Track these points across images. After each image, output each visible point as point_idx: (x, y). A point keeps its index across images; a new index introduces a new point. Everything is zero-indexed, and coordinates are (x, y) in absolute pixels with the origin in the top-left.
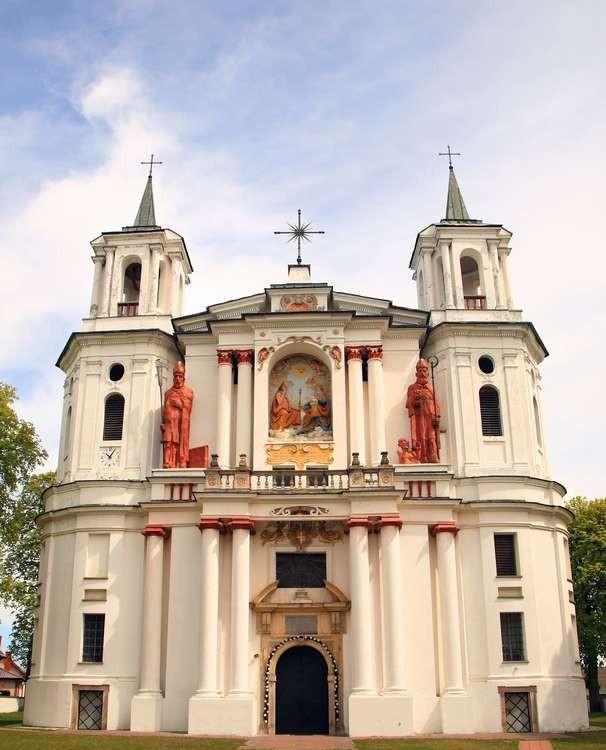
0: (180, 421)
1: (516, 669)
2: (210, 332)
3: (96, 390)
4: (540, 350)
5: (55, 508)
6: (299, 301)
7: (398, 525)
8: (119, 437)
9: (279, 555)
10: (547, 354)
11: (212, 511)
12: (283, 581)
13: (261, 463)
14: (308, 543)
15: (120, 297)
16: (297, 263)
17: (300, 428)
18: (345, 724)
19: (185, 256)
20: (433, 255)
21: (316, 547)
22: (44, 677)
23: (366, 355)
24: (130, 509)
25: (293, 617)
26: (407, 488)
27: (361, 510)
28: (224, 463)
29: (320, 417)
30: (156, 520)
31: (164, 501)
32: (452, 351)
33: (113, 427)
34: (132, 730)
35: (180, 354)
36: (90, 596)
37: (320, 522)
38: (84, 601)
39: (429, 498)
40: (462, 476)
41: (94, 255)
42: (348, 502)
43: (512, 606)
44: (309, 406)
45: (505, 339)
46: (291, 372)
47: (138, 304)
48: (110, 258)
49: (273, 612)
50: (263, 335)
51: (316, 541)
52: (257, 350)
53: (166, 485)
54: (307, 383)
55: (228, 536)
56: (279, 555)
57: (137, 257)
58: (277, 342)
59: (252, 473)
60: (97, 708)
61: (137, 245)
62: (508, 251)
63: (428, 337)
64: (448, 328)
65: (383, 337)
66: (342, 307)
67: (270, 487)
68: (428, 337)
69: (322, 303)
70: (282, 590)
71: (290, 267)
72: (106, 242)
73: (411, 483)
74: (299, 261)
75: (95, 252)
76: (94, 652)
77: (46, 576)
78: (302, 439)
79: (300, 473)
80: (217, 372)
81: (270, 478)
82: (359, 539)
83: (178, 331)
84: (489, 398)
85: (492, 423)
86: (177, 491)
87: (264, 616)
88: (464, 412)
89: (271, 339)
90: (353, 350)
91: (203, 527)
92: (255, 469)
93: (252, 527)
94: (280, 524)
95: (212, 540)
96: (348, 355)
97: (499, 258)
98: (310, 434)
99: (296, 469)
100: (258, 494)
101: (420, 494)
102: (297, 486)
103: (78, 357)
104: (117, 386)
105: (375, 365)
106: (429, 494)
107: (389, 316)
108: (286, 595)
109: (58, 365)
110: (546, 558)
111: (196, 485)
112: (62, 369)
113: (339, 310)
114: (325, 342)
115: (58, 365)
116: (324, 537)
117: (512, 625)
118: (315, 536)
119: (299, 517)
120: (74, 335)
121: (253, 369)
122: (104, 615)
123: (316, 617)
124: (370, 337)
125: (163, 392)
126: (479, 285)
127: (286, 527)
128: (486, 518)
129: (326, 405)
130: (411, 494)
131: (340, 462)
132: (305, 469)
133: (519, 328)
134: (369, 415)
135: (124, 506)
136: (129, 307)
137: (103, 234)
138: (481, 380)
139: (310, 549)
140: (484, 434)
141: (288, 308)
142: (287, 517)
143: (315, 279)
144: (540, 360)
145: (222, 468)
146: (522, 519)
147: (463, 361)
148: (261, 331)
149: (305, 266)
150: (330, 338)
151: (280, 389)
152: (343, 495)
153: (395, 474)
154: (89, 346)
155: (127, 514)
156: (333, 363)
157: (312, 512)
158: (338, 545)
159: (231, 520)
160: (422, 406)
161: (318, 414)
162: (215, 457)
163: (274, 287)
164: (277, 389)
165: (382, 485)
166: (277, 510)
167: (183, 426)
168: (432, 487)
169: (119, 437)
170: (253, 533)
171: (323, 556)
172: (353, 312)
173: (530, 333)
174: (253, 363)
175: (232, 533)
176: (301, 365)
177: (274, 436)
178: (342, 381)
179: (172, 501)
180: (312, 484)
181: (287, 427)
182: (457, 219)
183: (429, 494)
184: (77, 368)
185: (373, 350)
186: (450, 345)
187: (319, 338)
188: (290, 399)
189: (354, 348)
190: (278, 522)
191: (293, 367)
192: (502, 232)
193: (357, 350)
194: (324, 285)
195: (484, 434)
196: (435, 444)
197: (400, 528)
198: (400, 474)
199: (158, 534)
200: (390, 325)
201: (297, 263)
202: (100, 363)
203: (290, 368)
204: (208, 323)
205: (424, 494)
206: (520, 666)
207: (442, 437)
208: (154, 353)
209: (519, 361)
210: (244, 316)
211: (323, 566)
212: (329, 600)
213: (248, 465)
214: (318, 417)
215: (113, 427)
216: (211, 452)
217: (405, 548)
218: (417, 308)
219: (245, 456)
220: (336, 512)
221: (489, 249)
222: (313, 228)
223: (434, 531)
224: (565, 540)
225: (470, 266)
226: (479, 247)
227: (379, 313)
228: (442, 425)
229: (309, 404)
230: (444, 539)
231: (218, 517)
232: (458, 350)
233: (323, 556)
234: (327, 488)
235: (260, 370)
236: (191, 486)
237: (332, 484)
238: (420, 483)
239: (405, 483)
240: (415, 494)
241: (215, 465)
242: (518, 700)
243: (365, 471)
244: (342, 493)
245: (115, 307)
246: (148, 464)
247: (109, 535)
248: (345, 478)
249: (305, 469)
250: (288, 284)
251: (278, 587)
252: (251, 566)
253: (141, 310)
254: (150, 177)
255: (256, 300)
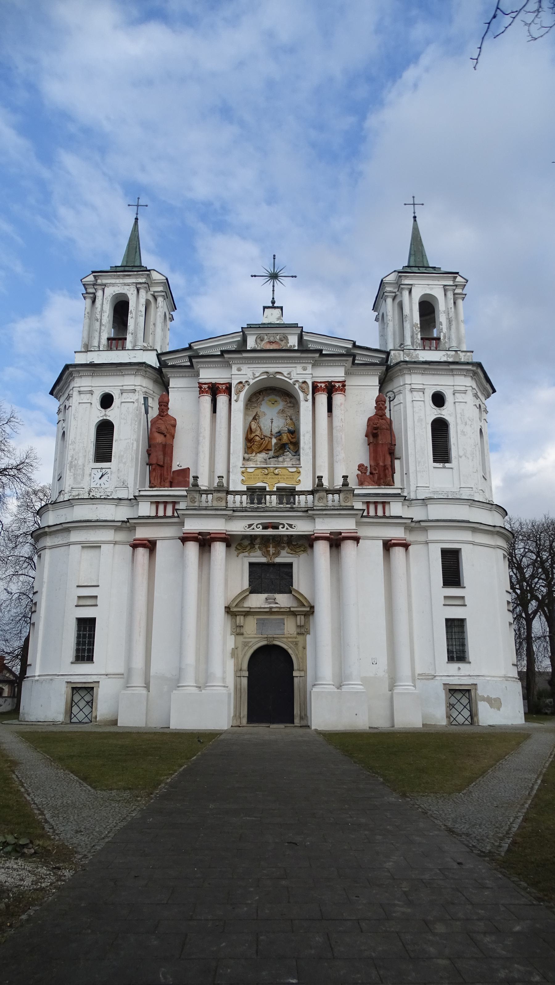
0: (161, 474)
1: (459, 669)
2: (192, 366)
3: (85, 416)
4: (487, 387)
5: (51, 523)
6: (272, 339)
7: (357, 539)
8: (109, 460)
9: (251, 564)
10: (494, 391)
11: (193, 525)
12: (254, 589)
13: (237, 483)
14: (277, 554)
15: (107, 331)
16: (271, 305)
17: (271, 453)
18: (308, 715)
19: (168, 294)
20: (394, 298)
21: (284, 558)
22: (39, 676)
23: (331, 389)
24: (119, 524)
25: (264, 620)
26: (364, 507)
27: (324, 526)
28: (203, 483)
29: (289, 443)
30: (142, 533)
31: (149, 517)
32: (408, 387)
33: (103, 451)
34: (119, 724)
35: (163, 383)
36: (82, 602)
37: (287, 536)
38: (76, 606)
39: (384, 517)
40: (414, 498)
41: (85, 292)
42: (312, 518)
43: (456, 613)
44: (279, 433)
45: (457, 378)
46: (263, 403)
47: (126, 339)
48: (99, 294)
49: (248, 613)
50: (239, 370)
51: (283, 553)
52: (234, 383)
53: (151, 502)
54: (278, 413)
55: (207, 548)
56: (251, 564)
57: (125, 295)
58: (252, 377)
59: (228, 492)
60: (88, 703)
61: (125, 284)
62: (463, 296)
63: (388, 371)
64: (405, 366)
65: (347, 373)
66: (311, 346)
67: (244, 505)
68: (388, 371)
69: (293, 341)
70: (253, 596)
71: (265, 308)
72: (96, 280)
73: (368, 503)
74: (273, 302)
75: (86, 289)
76: (85, 651)
77: (41, 586)
78: (272, 464)
79: (271, 493)
80: (182, 556)
81: (244, 497)
82: (322, 549)
83: (163, 364)
84: (440, 428)
85: (441, 453)
86: (161, 507)
87: (238, 617)
88: (416, 440)
89: (246, 374)
90: (319, 385)
91: (184, 539)
92: (231, 489)
93: (228, 540)
94: (252, 538)
95: (192, 548)
96: (315, 389)
97: (455, 303)
98: (281, 459)
99: (268, 489)
100: (234, 511)
101: (376, 513)
102: (268, 504)
103: (71, 387)
104: (107, 413)
105: (338, 398)
106: (384, 513)
107: (352, 356)
108: (258, 601)
109: (51, 393)
110: (488, 574)
111: (179, 503)
112: (56, 397)
113: (308, 350)
114: (295, 377)
115: (51, 393)
116: (289, 551)
117: (456, 628)
118: (283, 548)
119: (270, 532)
120: (67, 367)
121: (230, 400)
122: (94, 619)
123: (283, 619)
124: (335, 373)
125: (149, 420)
126: (434, 327)
127: (258, 541)
128: (433, 535)
129: (294, 433)
130: (368, 513)
131: (306, 483)
132: (275, 489)
133: (470, 367)
134: (332, 444)
135: (114, 521)
136: (117, 341)
137: (93, 272)
138: (433, 413)
139: (278, 560)
140: (435, 461)
141: (264, 345)
142: (259, 531)
143: (286, 320)
144: (488, 396)
145: (203, 488)
146: (467, 536)
147: (418, 396)
148: (238, 366)
149: (278, 307)
150: (298, 373)
151: (254, 419)
152: (309, 513)
153: (354, 495)
154: (81, 376)
155: (117, 529)
156: (301, 395)
157: (281, 526)
158: (303, 556)
159: (209, 534)
160: (381, 435)
161: (287, 441)
162: (196, 478)
163: (250, 327)
164: (251, 418)
165: (343, 504)
166: (250, 526)
167: (167, 450)
168: (387, 507)
169: (109, 460)
170: (228, 546)
171: (290, 565)
172: (320, 351)
173: (479, 371)
174: (230, 395)
175: (210, 546)
176: (273, 397)
177: (248, 460)
178: (310, 415)
179: (157, 517)
180: (281, 503)
181: (260, 452)
182: (418, 263)
183: (384, 513)
184: (69, 397)
185: (337, 385)
186: (407, 383)
187: (289, 374)
188: (262, 427)
189: (321, 382)
190: (251, 536)
191: (266, 398)
192: (459, 279)
193: (323, 385)
194: (295, 326)
195: (435, 461)
196: (390, 469)
197: (358, 543)
198: (359, 495)
199: (144, 546)
200: (353, 363)
201: (271, 305)
202: (91, 392)
203: (263, 400)
204: (190, 358)
205: (380, 513)
206: (461, 665)
207: (397, 462)
208: (140, 383)
209: (469, 398)
210: (222, 352)
211: (290, 575)
212: (295, 605)
213: (225, 485)
214: (287, 444)
215: (103, 451)
216: (192, 474)
217: (363, 558)
218: (378, 348)
219: (223, 477)
220: (302, 527)
221: (445, 295)
222: (262, 280)
223: (388, 545)
224: (505, 557)
225: (427, 308)
226: (438, 293)
227: (344, 352)
228: (397, 454)
229: (279, 432)
230: (398, 552)
231: (198, 531)
232: (413, 386)
233: (290, 565)
234: (294, 506)
235: (236, 401)
236: (174, 503)
237: (299, 503)
238: (376, 503)
239: (363, 502)
240: (372, 513)
241: (196, 485)
242: (461, 695)
243: (328, 492)
244: (307, 511)
245: (104, 341)
246: (135, 483)
247: (100, 547)
248: (310, 497)
249: (275, 489)
250: (262, 324)
251: (251, 592)
252: (229, 574)
253: (129, 345)
254: (137, 219)
255: (233, 337)
